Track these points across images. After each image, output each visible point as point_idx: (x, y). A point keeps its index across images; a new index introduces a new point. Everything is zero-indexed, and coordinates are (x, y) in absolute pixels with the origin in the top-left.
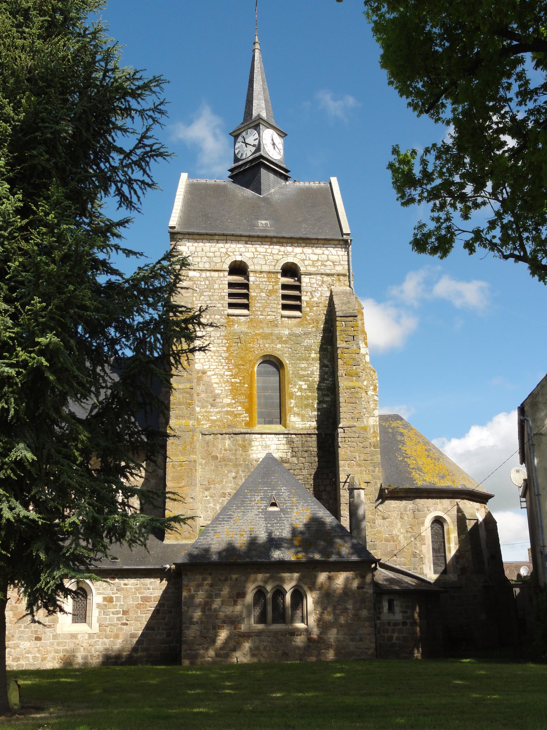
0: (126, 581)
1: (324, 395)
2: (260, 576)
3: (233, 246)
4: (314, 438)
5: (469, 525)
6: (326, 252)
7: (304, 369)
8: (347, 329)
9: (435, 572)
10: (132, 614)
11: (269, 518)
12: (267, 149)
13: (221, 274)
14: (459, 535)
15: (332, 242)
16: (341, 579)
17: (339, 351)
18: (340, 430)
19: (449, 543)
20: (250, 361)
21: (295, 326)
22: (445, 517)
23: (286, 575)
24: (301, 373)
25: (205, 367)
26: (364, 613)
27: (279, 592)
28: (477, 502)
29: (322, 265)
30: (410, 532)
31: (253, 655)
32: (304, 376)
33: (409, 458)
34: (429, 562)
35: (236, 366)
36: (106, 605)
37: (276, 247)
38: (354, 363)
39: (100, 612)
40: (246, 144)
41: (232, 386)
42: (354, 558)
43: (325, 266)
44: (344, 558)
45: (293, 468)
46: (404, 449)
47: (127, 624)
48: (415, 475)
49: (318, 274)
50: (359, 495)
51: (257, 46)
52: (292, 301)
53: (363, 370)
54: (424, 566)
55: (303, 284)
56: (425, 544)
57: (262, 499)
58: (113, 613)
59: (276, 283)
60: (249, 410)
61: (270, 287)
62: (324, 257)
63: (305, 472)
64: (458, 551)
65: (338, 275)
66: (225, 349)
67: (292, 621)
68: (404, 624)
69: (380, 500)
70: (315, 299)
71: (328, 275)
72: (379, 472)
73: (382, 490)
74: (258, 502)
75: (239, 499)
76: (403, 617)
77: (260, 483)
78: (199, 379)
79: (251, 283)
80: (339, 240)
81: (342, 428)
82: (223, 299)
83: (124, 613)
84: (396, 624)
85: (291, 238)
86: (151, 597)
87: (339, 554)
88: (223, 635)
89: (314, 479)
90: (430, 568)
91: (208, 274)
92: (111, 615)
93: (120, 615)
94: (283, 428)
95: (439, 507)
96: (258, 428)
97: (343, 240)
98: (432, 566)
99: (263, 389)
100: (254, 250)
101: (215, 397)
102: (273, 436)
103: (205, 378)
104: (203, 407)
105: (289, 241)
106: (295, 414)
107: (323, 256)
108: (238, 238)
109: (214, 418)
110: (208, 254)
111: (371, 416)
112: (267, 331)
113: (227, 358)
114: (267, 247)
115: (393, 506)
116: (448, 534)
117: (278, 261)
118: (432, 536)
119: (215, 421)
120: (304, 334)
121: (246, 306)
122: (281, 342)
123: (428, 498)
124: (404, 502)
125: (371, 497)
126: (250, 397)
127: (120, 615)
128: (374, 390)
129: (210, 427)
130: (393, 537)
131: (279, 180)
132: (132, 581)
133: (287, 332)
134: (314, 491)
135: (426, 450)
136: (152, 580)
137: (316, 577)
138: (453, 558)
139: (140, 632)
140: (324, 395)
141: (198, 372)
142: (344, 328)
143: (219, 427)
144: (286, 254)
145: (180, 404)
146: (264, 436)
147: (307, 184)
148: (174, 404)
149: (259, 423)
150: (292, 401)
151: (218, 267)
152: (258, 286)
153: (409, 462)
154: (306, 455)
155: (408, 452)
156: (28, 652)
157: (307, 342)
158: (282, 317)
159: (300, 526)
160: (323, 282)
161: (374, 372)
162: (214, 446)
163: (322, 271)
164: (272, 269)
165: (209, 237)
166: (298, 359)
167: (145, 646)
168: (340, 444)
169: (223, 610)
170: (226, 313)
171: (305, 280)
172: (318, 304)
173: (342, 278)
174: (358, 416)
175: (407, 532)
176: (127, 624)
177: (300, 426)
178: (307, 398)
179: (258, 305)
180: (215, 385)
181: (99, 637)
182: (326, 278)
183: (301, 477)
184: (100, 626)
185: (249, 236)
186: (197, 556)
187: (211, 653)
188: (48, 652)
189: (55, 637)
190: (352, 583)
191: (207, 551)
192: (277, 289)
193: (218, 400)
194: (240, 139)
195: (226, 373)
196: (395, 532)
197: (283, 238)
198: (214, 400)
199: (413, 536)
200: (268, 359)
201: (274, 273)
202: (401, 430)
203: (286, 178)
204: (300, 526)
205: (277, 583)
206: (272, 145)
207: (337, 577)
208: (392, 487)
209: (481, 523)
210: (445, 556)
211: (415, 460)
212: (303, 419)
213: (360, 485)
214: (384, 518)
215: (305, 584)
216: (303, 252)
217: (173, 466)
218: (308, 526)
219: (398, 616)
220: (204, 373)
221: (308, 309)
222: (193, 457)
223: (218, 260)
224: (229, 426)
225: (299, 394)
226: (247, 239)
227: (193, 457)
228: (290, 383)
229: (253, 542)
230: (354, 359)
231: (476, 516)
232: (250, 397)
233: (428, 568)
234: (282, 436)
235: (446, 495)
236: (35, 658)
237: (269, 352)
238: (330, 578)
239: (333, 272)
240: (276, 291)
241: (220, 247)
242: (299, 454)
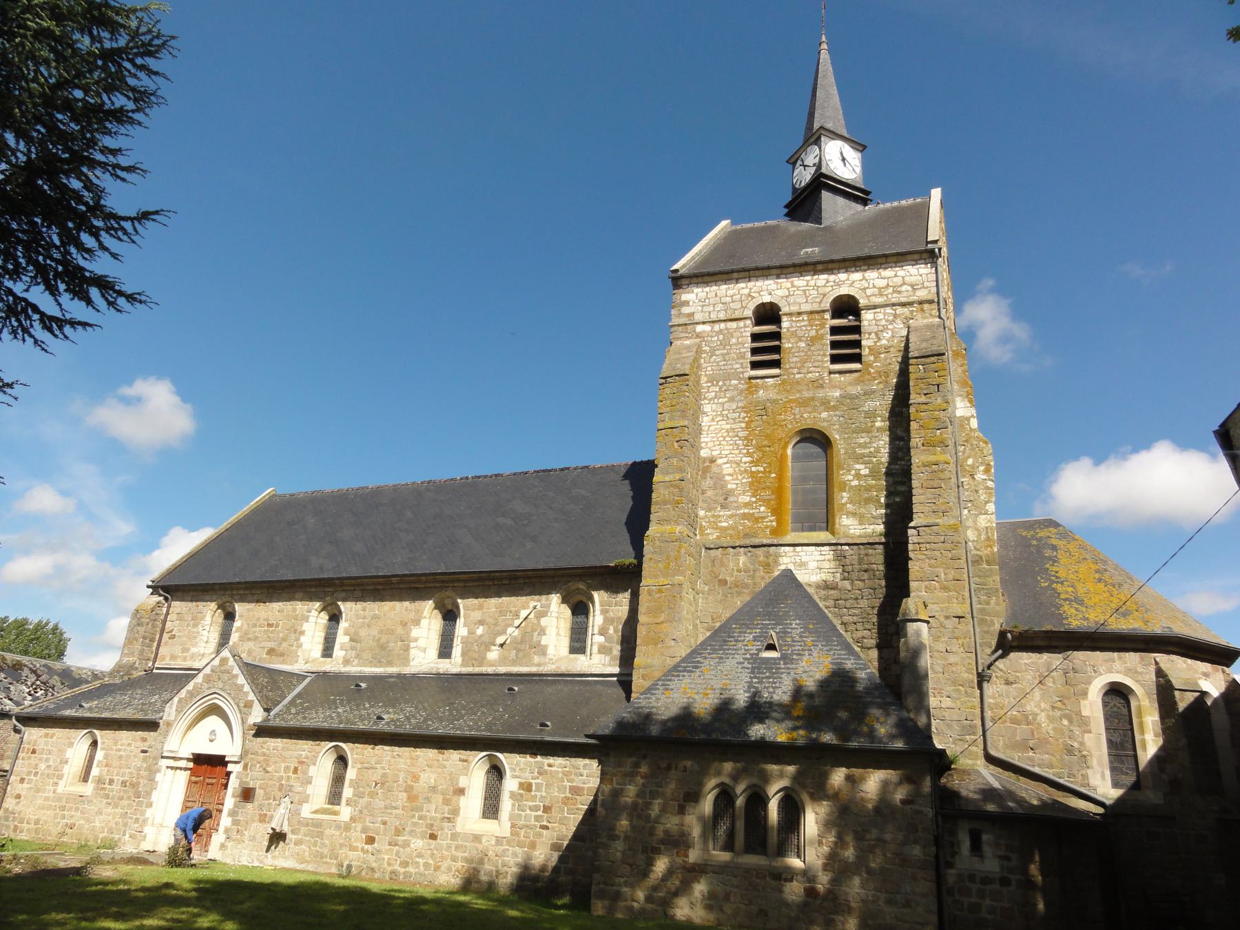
0: (551, 760)
1: (896, 483)
2: (728, 766)
3: (759, 283)
4: (880, 549)
5: (1182, 699)
6: (901, 272)
7: (865, 446)
8: (927, 375)
9: (1116, 785)
10: (555, 813)
11: (759, 668)
12: (832, 166)
13: (741, 324)
14: (1162, 718)
15: (909, 257)
16: (873, 782)
17: (912, 410)
18: (910, 532)
19: (1142, 732)
20: (780, 440)
21: (850, 384)
22: (1128, 681)
23: (774, 768)
24: (858, 451)
25: (714, 453)
26: (916, 851)
27: (758, 800)
28: (1203, 660)
29: (894, 291)
30: (1060, 709)
31: (709, 907)
32: (863, 456)
33: (1062, 583)
34: (1100, 764)
35: (759, 448)
36: (522, 795)
37: (822, 277)
38: (938, 424)
39: (513, 805)
40: (805, 166)
41: (752, 477)
42: (899, 745)
43: (899, 292)
44: (880, 741)
45: (844, 596)
46: (1055, 569)
47: (547, 828)
48: (1068, 610)
49: (887, 305)
50: (918, 633)
51: (824, 46)
52: (846, 348)
53: (967, 441)
54: (1089, 772)
55: (865, 323)
56: (1090, 732)
57: (755, 639)
58: (531, 809)
59: (822, 326)
60: (777, 511)
61: (813, 333)
62: (898, 280)
63: (864, 603)
64: (1162, 749)
65: (921, 303)
66: (743, 425)
67: (781, 851)
68: (1005, 882)
69: (1000, 652)
70: (884, 342)
71: (904, 305)
72: (997, 604)
73: (1002, 634)
74: (748, 642)
75: (720, 638)
76: (1002, 868)
77: (759, 614)
78: (706, 470)
79: (784, 330)
80: (921, 252)
81: (914, 528)
82: (743, 357)
83: (547, 809)
84: (986, 880)
85: (844, 260)
86: (583, 789)
87: (871, 735)
88: (661, 865)
89: (879, 615)
90: (1103, 776)
91: (723, 325)
92: (528, 812)
93: (540, 813)
94: (830, 536)
95: (1117, 665)
96: (791, 537)
97: (927, 251)
98: (1108, 773)
99: (801, 479)
100: (789, 285)
101: (728, 494)
102: (813, 548)
103: (714, 469)
104: (709, 510)
105: (842, 265)
106: (849, 514)
107: (895, 279)
108: (766, 272)
109: (725, 524)
110: (724, 300)
111: (981, 514)
112: (806, 395)
113: (746, 438)
114: (808, 278)
115: (1025, 662)
116: (1140, 716)
117: (824, 295)
118: (1106, 719)
119: (725, 529)
120: (865, 394)
121: (776, 364)
122: (828, 409)
123: (1093, 649)
124: (1046, 656)
125: (966, 641)
126: (779, 492)
127: (540, 813)
128: (987, 471)
129: (718, 537)
130: (1026, 717)
131: (854, 204)
132: (559, 761)
133: (837, 394)
134: (878, 633)
135: (1097, 571)
136: (587, 761)
137: (825, 776)
138: (1151, 762)
139: (566, 843)
140: (896, 483)
141: (704, 460)
142: (921, 374)
143: (731, 536)
144: (838, 284)
145: (665, 503)
146: (799, 549)
147: (896, 204)
148: (657, 503)
149: (794, 530)
150: (845, 494)
151: (737, 315)
152: (794, 334)
153: (1059, 588)
154: (866, 576)
155: (1062, 574)
156: (420, 856)
157: (869, 405)
158: (831, 373)
159: (810, 684)
160: (895, 316)
161: (986, 443)
162: (722, 564)
163: (894, 300)
164: (816, 307)
165: (725, 276)
166: (854, 432)
167: (570, 865)
168: (911, 555)
169: (663, 820)
170: (746, 375)
171: (867, 316)
172: (887, 350)
173: (926, 306)
174: (943, 507)
175: (1053, 708)
176: (547, 828)
177: (858, 532)
178: (869, 489)
179: (795, 359)
180: (727, 478)
181: (509, 843)
182: (900, 310)
183: (857, 612)
184: (513, 826)
185: (781, 267)
186: (634, 725)
187: (641, 895)
188: (443, 858)
189: (454, 836)
190: (893, 793)
191: (648, 717)
192: (822, 335)
193: (731, 499)
194: (799, 162)
195: (745, 459)
196: (1030, 707)
197: (832, 261)
198: (725, 499)
199: (1066, 716)
200: (808, 435)
201: (818, 312)
202: (1054, 542)
203: (865, 202)
204: (810, 684)
205: (755, 781)
206: (841, 160)
207: (863, 779)
208: (1022, 628)
209: (1216, 701)
210: (1135, 756)
211: (1072, 586)
212: (862, 523)
213: (917, 613)
214: (1008, 683)
215: (803, 786)
216: (864, 278)
217: (650, 593)
218: (824, 684)
219: (991, 865)
220: (713, 461)
221: (872, 358)
222: (679, 578)
223: (737, 305)
224: (746, 535)
225: (855, 483)
226: (778, 271)
227: (679, 578)
228: (840, 467)
229: (724, 707)
230: (937, 419)
231: (1197, 684)
232: (779, 492)
233: (1099, 776)
234: (827, 548)
235: (1132, 646)
236: (426, 865)
237: (809, 424)
238: (849, 778)
239: (911, 299)
240: (822, 337)
241: (743, 288)
242: (855, 575)
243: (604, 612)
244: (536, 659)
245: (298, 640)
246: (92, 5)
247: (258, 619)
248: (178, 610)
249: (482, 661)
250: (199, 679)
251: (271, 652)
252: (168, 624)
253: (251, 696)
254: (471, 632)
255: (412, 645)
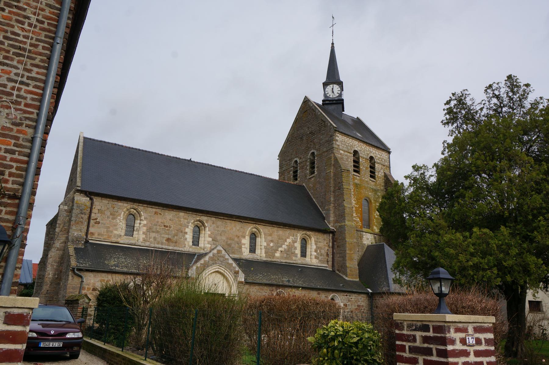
243: (316, 244)
244: (294, 258)
245: (184, 236)
246: (414, 167)
247: (158, 222)
248: (99, 208)
249: (274, 256)
250: (207, 258)
251: (168, 240)
252: (93, 215)
253: (237, 269)
254: (268, 245)
255: (243, 246)
